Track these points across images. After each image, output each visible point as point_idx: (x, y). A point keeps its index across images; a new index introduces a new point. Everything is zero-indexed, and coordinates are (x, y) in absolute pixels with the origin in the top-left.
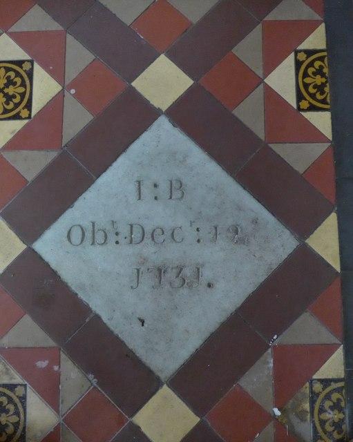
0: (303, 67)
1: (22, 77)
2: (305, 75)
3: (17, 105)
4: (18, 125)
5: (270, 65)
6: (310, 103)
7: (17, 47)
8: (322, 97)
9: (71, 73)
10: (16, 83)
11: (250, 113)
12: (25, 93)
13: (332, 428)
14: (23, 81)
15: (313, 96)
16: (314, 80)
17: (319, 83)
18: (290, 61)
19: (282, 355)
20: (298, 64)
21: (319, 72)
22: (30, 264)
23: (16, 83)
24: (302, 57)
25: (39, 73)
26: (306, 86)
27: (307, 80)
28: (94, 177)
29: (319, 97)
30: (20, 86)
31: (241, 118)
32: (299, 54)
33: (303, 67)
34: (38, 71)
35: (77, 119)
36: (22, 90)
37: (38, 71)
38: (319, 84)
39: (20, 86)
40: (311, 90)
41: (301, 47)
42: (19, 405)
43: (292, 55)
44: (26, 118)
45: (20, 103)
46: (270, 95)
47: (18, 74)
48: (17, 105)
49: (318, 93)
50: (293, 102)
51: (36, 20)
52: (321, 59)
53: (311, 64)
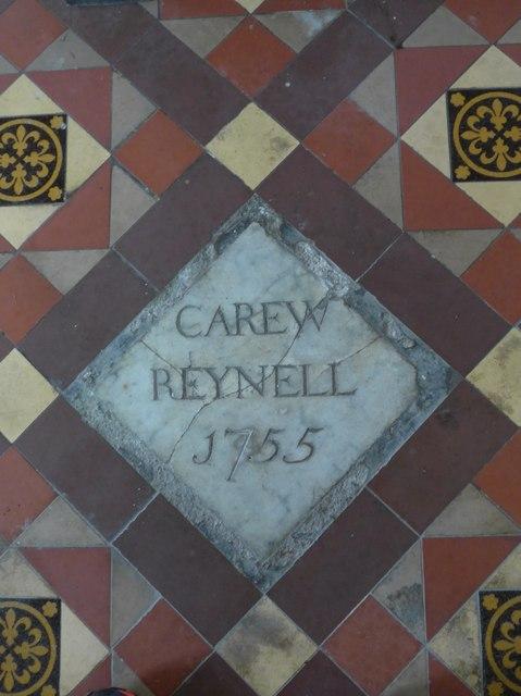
2: (464, 127)
3: (468, 110)
5: (407, 118)
6: (42, 612)
7: (40, 93)
8: (489, 161)
9: (394, 151)
10: (511, 658)
11: (382, 189)
12: (55, 162)
13: (41, 144)
14: (499, 660)
15: (475, 159)
16: (10, 627)
17: (14, 666)
18: (440, 106)
19: (103, 244)
20: (452, 111)
21: (22, 664)
22: (60, 419)
23: (511, 658)
24: (458, 100)
26: (465, 144)
27: (466, 135)
28: (368, 489)
29: (484, 160)
30: (470, 141)
31: (369, 197)
32: (453, 96)
34: (75, 130)
35: (130, 203)
37: (75, 130)
38: (485, 140)
39: (470, 141)
40: (473, 150)
41: (457, 85)
42: (461, 152)
43: (443, 98)
46: (410, 158)
48: (43, 181)
49: (484, 154)
50: (444, 167)
51: (69, 52)
52: (489, 103)
53: (472, 112)
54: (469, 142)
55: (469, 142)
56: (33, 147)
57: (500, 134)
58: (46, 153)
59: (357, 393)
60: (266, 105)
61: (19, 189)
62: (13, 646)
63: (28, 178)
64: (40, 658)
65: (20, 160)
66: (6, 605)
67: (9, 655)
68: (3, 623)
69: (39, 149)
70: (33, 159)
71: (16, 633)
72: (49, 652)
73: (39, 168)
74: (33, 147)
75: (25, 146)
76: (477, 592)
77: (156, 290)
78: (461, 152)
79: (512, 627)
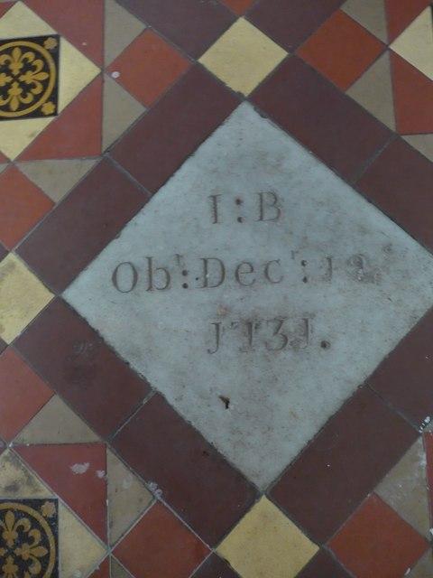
0: (31, 511)
1: (43, 59)
4: (39, 125)
13: (34, 63)
16: (10, 530)
17: (29, 73)
25: (68, 52)
31: (360, 101)
33: (31, 511)
34: (68, 52)
36: (43, 76)
42: (48, 531)
44: (50, 115)
45: (41, 95)
47: (38, 55)
48: (37, 98)
54: (43, 70)
55: (43, 70)
56: (28, 67)
57: (16, 78)
58: (41, 71)
59: (226, 396)
60: (258, 21)
61: (14, 106)
62: (18, 81)
63: (24, 95)
64: (40, 559)
65: (16, 78)
66: (4, 506)
67: (15, 551)
68: (3, 525)
69: (34, 68)
70: (28, 78)
71: (29, 82)
72: (49, 554)
73: (33, 86)
74: (28, 67)
75: (10, 91)
76: (57, 497)
77: (149, 193)
78: (48, 531)
79: (31, 569)
